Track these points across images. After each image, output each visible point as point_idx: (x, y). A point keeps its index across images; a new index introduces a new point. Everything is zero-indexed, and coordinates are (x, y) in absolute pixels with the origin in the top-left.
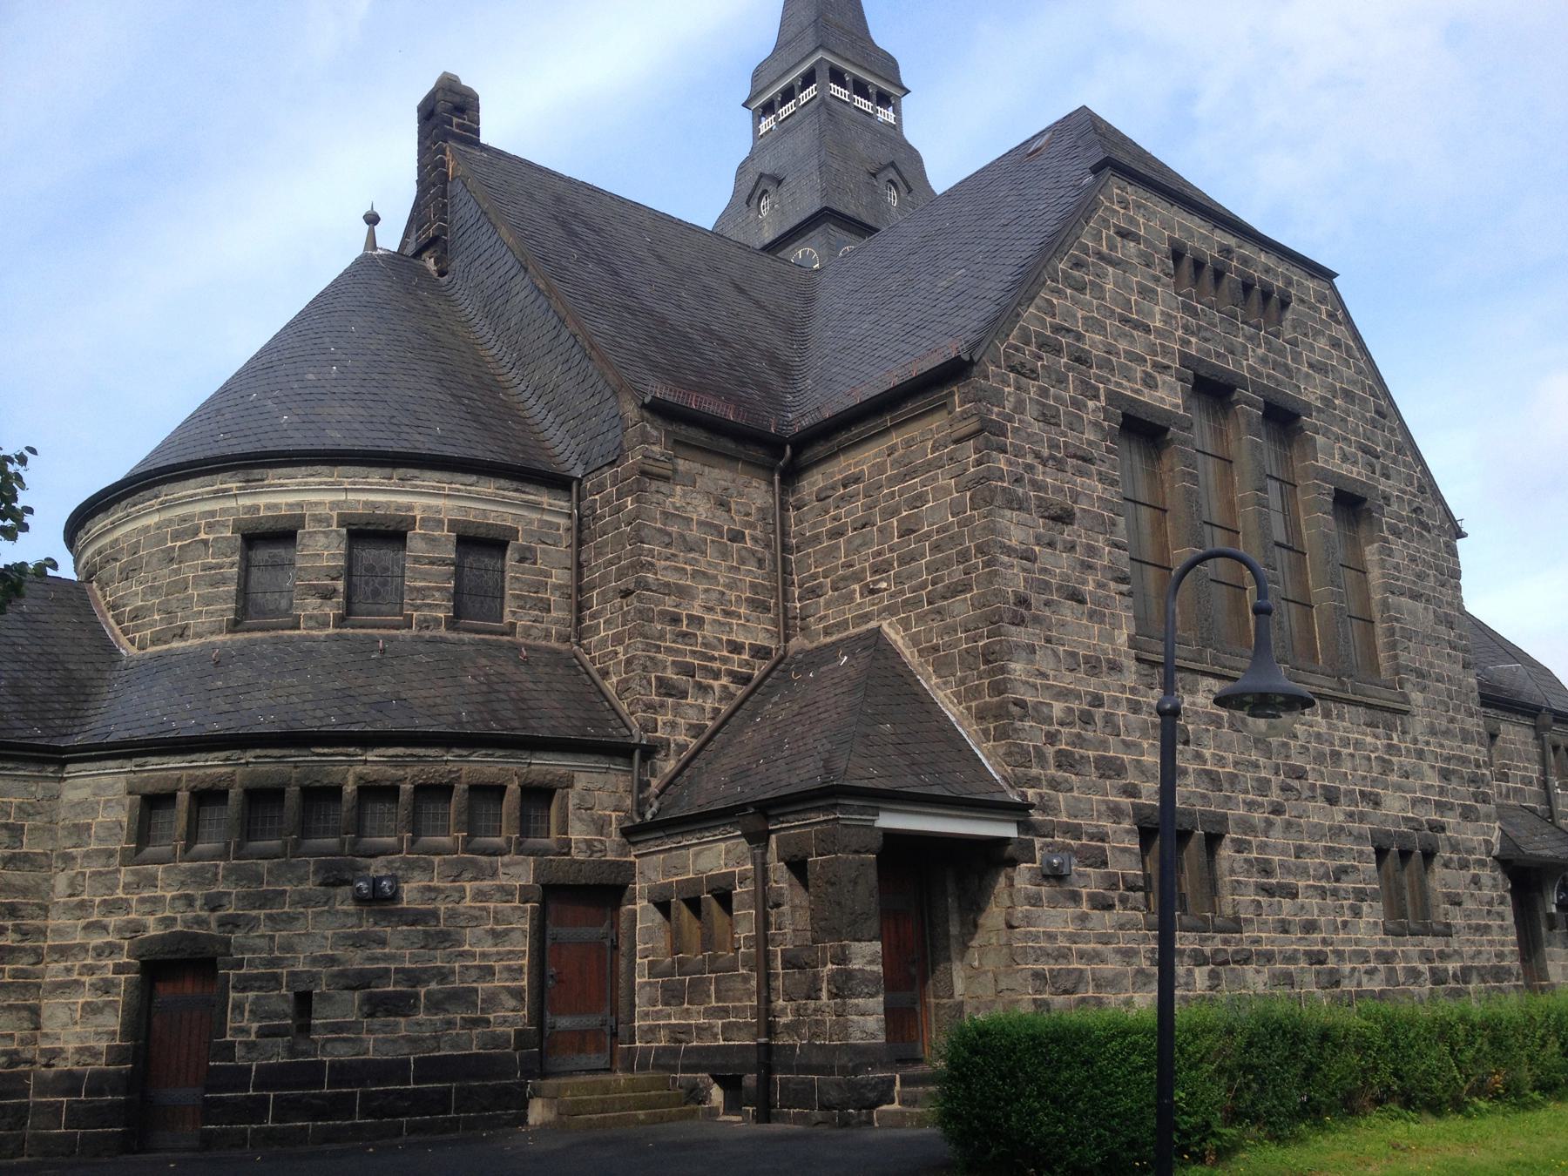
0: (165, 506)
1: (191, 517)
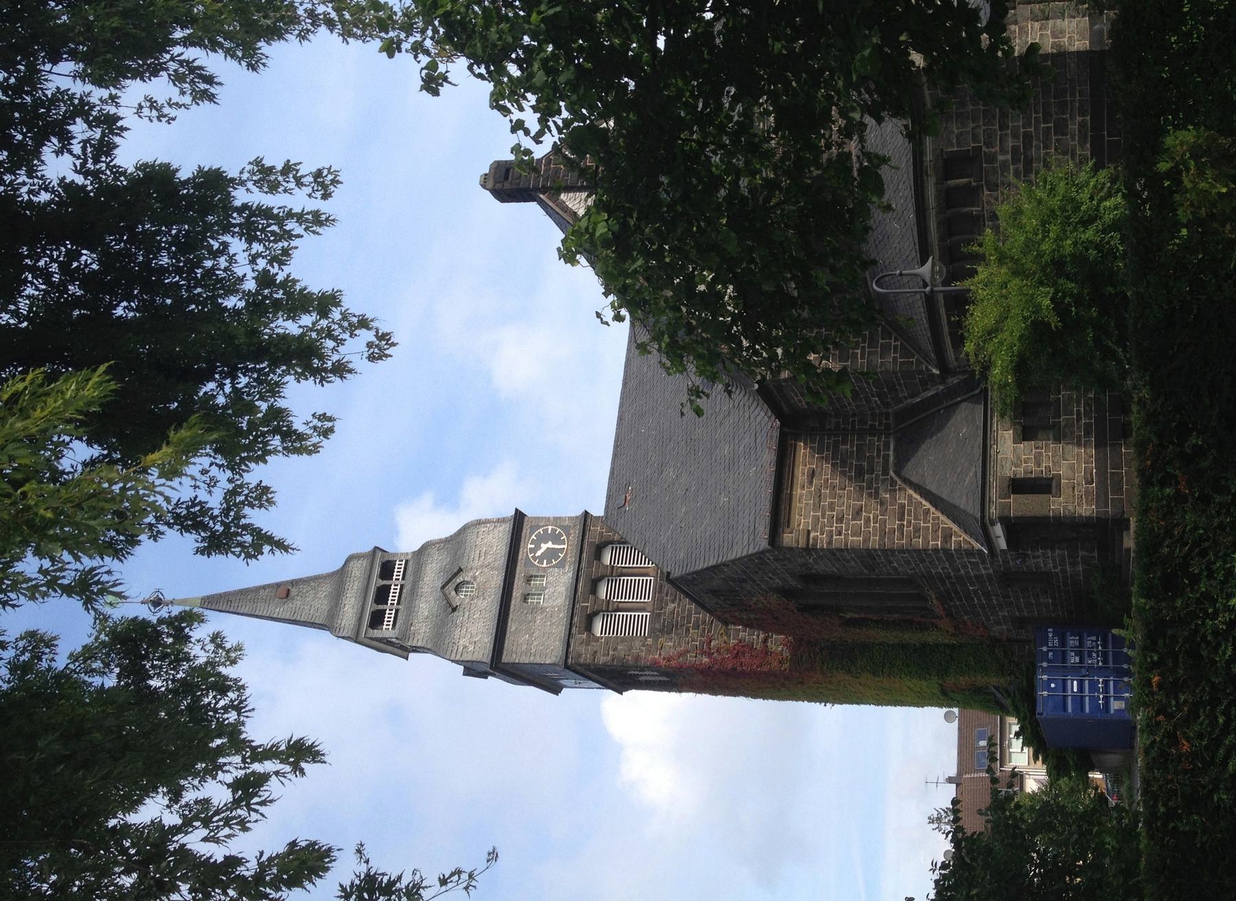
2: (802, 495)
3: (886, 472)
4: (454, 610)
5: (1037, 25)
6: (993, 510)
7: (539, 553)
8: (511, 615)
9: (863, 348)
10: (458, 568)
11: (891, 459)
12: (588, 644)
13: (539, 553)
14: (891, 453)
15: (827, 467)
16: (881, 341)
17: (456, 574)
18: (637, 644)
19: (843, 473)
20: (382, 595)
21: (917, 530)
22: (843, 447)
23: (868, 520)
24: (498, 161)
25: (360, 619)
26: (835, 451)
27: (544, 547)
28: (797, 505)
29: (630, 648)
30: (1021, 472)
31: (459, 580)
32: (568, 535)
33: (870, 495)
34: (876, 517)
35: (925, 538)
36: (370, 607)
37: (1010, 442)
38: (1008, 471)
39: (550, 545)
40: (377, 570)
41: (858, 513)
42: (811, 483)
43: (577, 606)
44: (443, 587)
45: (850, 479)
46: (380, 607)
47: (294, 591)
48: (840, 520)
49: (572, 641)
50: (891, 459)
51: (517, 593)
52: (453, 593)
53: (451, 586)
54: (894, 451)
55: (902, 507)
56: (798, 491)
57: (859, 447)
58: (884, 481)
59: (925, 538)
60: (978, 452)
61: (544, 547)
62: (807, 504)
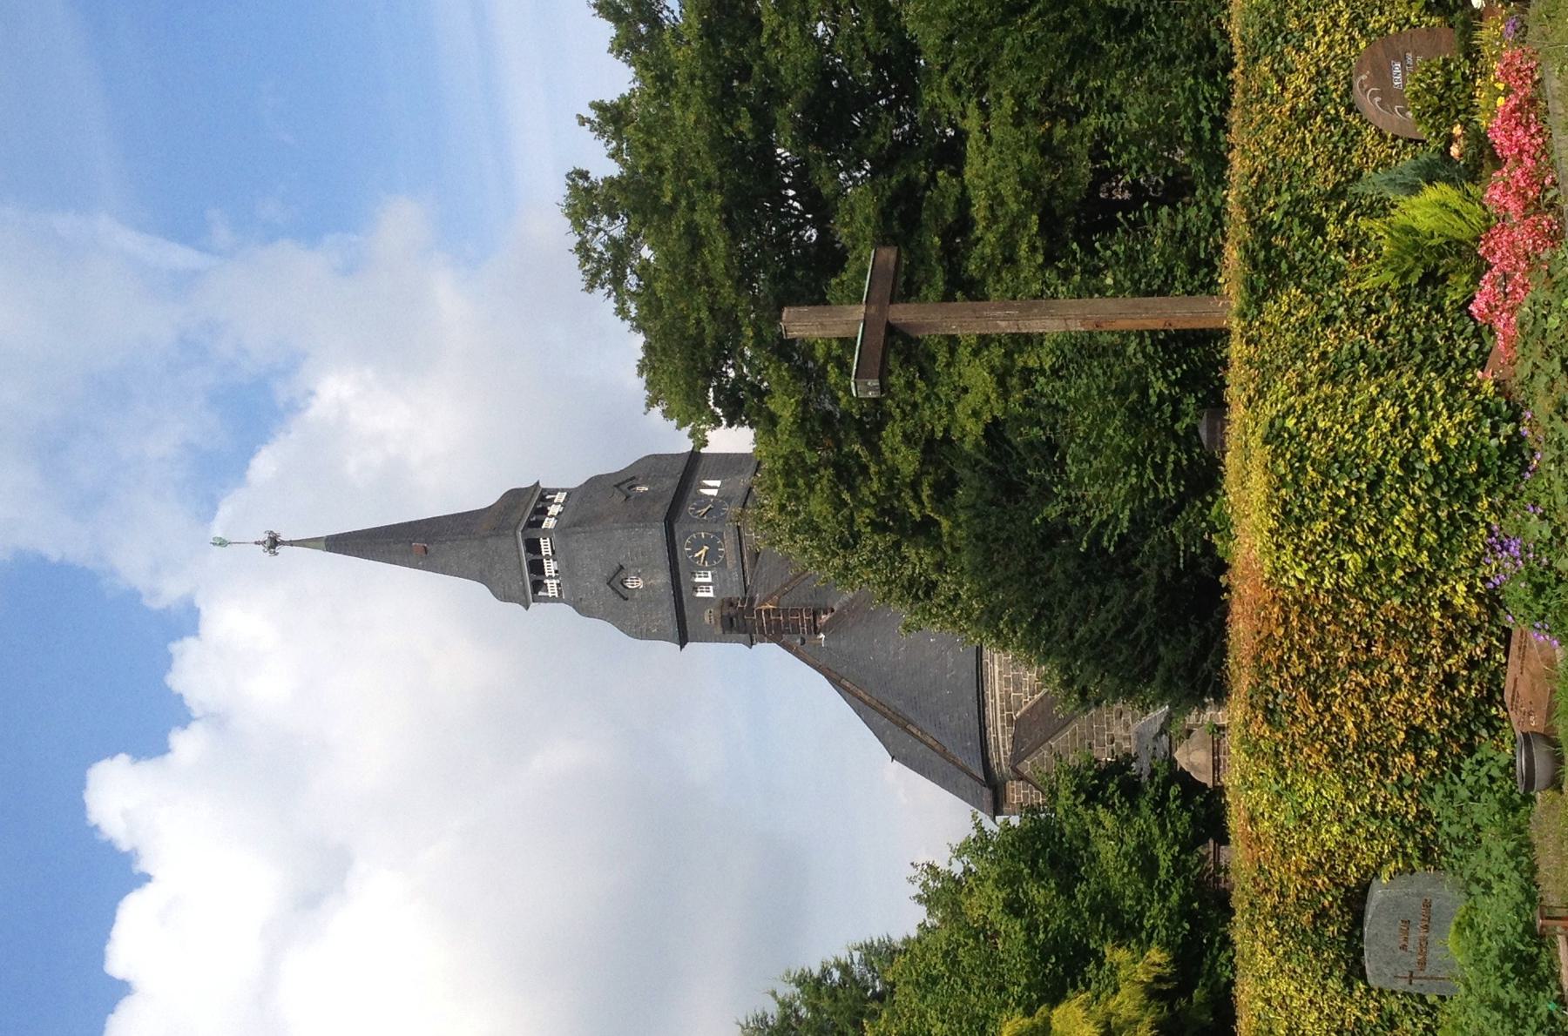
31: (622, 576)
40: (523, 548)
53: (616, 582)
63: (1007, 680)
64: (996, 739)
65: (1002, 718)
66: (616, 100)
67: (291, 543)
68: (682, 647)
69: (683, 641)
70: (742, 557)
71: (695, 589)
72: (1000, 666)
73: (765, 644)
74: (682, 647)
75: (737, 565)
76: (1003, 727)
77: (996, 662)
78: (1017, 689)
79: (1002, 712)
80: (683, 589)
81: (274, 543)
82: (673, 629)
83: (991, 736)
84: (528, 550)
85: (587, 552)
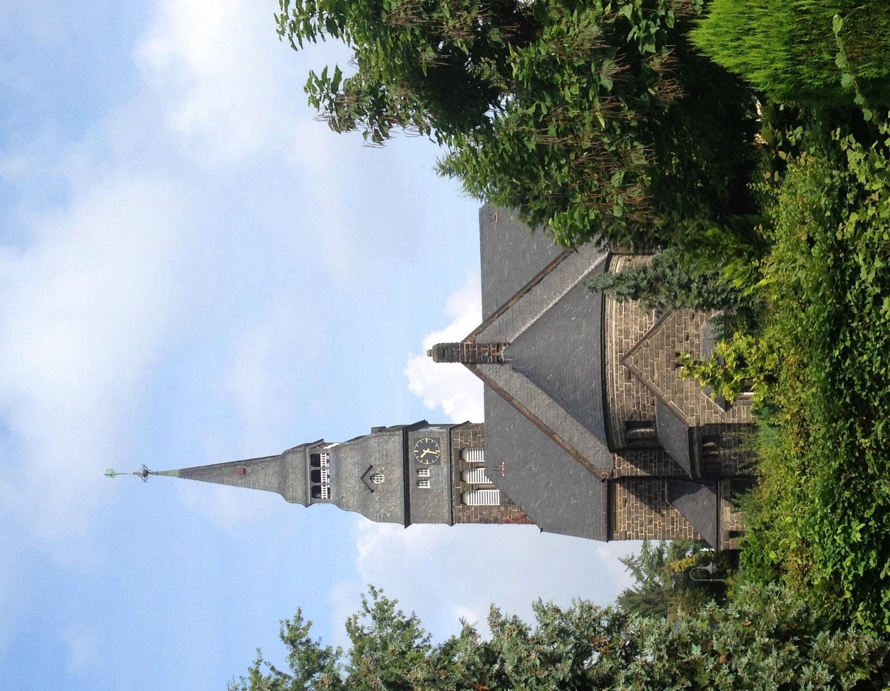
0: (611, 317)
1: (616, 309)
2: (621, 512)
3: (663, 500)
4: (372, 491)
5: (745, 407)
6: (722, 547)
7: (422, 456)
8: (411, 495)
9: (655, 463)
10: (369, 466)
11: (666, 493)
12: (464, 511)
13: (422, 456)
14: (666, 489)
15: (632, 497)
16: (664, 460)
17: (369, 470)
18: (495, 511)
19: (641, 500)
20: (316, 476)
21: (681, 531)
22: (640, 487)
23: (655, 525)
24: (438, 345)
25: (306, 494)
26: (636, 490)
27: (425, 452)
28: (618, 518)
29: (490, 513)
30: (734, 528)
31: (372, 473)
32: (419, 439)
33: (656, 511)
34: (660, 524)
35: (685, 534)
36: (310, 484)
37: (729, 514)
38: (728, 527)
39: (428, 451)
40: (309, 461)
41: (650, 522)
42: (625, 506)
43: (453, 489)
44: (362, 478)
45: (645, 503)
46: (317, 484)
47: (248, 470)
48: (642, 525)
49: (454, 510)
50: (666, 493)
51: (412, 482)
52: (370, 481)
54: (668, 489)
55: (673, 518)
56: (618, 511)
57: (649, 487)
58: (663, 505)
59: (685, 534)
60: (714, 518)
61: (425, 452)
62: (624, 517)
63: (620, 331)
64: (612, 374)
65: (616, 358)
66: (432, 358)
67: (153, 473)
68: (405, 527)
69: (407, 523)
70: (451, 455)
71: (418, 484)
72: (616, 321)
73: (444, 364)
74: (405, 527)
75: (448, 475)
76: (617, 365)
77: (614, 319)
78: (627, 337)
79: (616, 353)
80: (410, 477)
81: (146, 473)
82: (400, 511)
83: (608, 371)
84: (312, 464)
85: (350, 460)
